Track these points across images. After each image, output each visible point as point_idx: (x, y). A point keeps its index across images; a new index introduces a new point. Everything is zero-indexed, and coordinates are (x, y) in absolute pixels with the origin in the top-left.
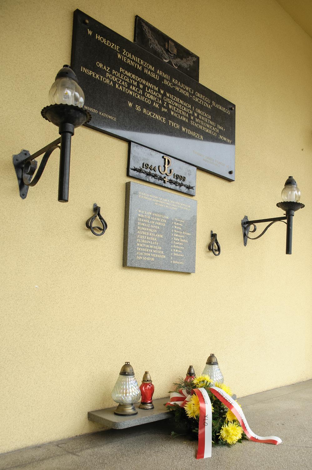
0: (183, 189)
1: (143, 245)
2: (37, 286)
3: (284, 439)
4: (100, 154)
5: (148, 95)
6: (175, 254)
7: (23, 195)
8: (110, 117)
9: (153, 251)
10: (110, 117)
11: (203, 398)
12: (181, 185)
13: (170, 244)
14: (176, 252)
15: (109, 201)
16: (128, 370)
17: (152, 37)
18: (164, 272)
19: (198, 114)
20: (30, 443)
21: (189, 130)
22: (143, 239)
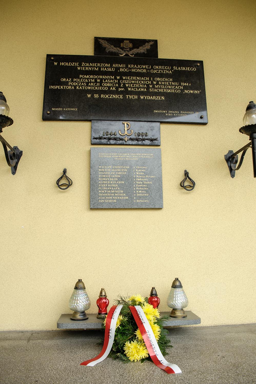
0: (147, 142)
1: (104, 192)
2: (23, 227)
3: (186, 371)
4: (68, 135)
5: (105, 85)
6: (138, 195)
7: (14, 173)
8: (72, 109)
9: (114, 195)
10: (72, 109)
11: (113, 314)
12: (144, 140)
13: (132, 187)
14: (139, 193)
15: (76, 164)
16: (81, 284)
17: (108, 45)
18: (129, 209)
19: (158, 82)
20: (19, 328)
21: (148, 96)
22: (104, 187)
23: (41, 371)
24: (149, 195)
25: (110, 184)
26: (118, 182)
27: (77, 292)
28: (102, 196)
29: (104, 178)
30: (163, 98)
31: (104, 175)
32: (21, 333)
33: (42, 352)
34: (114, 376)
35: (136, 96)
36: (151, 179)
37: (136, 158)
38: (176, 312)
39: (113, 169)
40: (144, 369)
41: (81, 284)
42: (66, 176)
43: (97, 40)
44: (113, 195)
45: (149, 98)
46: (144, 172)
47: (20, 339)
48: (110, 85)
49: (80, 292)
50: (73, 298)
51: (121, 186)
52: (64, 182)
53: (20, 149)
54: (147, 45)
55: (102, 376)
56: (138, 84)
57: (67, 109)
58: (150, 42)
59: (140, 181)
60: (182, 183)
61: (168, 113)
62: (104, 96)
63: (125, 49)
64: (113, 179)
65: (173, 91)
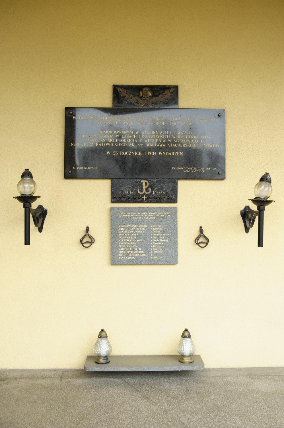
6: (155, 252)
14: (155, 250)
23: (75, 408)
24: (165, 252)
25: (129, 242)
26: (137, 240)
27: (100, 340)
28: (122, 253)
29: (124, 236)
30: (181, 154)
31: (123, 233)
32: (54, 371)
33: (73, 391)
34: (128, 413)
35: (154, 153)
36: (167, 238)
37: (154, 217)
38: (184, 358)
39: (132, 228)
40: (150, 408)
41: (103, 333)
42: (88, 234)
43: (116, 88)
44: (132, 252)
45: (167, 154)
46: (161, 231)
47: (54, 378)
48: (129, 140)
49: (103, 340)
50: (97, 344)
51: (139, 244)
52: (87, 240)
53: (44, 208)
54: (168, 93)
55: (119, 412)
56: (157, 139)
57: (88, 168)
58: (170, 89)
59: (156, 239)
60: (197, 241)
61: (185, 170)
62: (123, 153)
63: (145, 99)
64: (132, 237)
65: (191, 146)
